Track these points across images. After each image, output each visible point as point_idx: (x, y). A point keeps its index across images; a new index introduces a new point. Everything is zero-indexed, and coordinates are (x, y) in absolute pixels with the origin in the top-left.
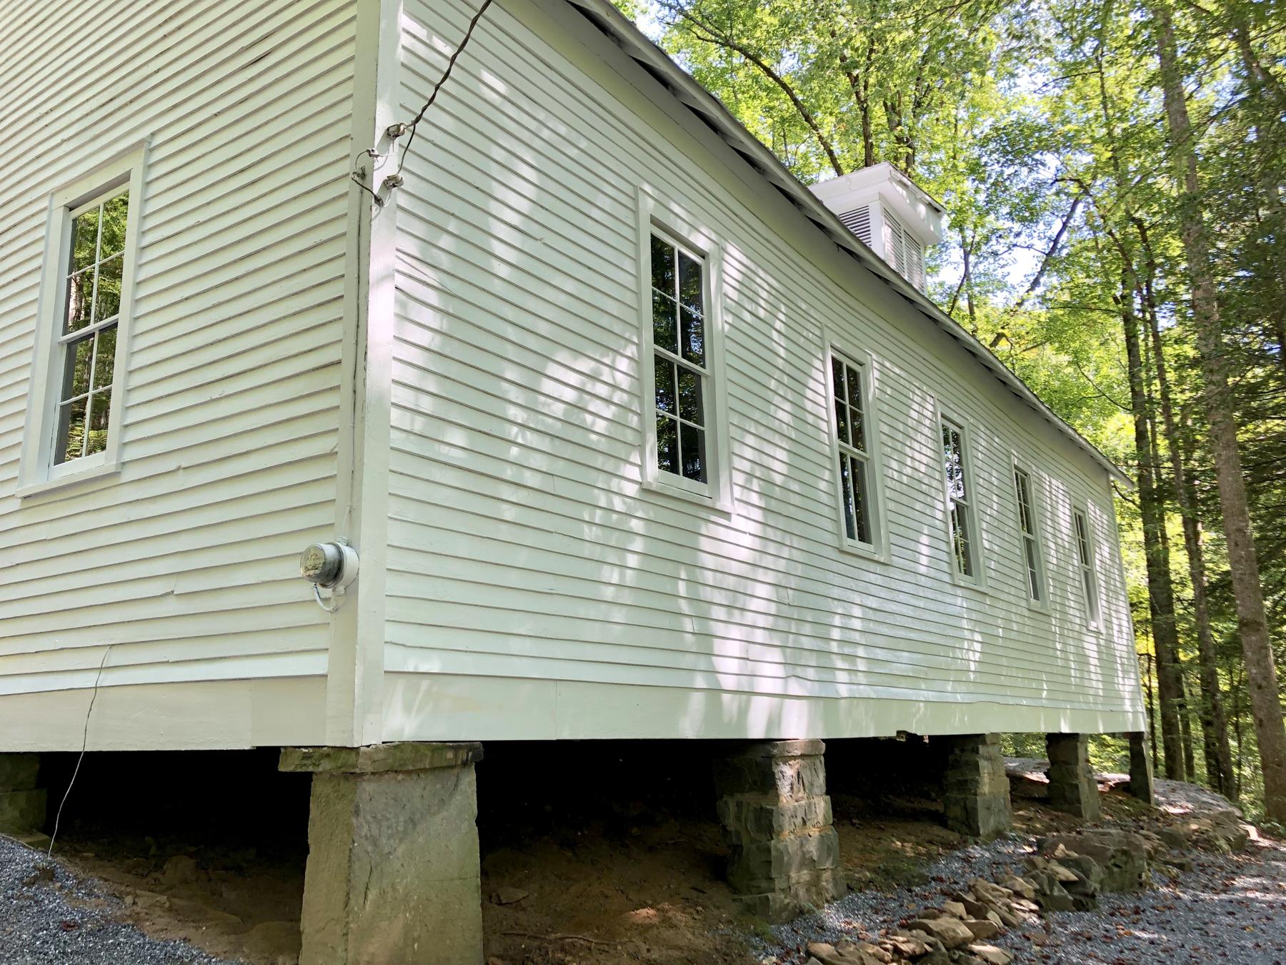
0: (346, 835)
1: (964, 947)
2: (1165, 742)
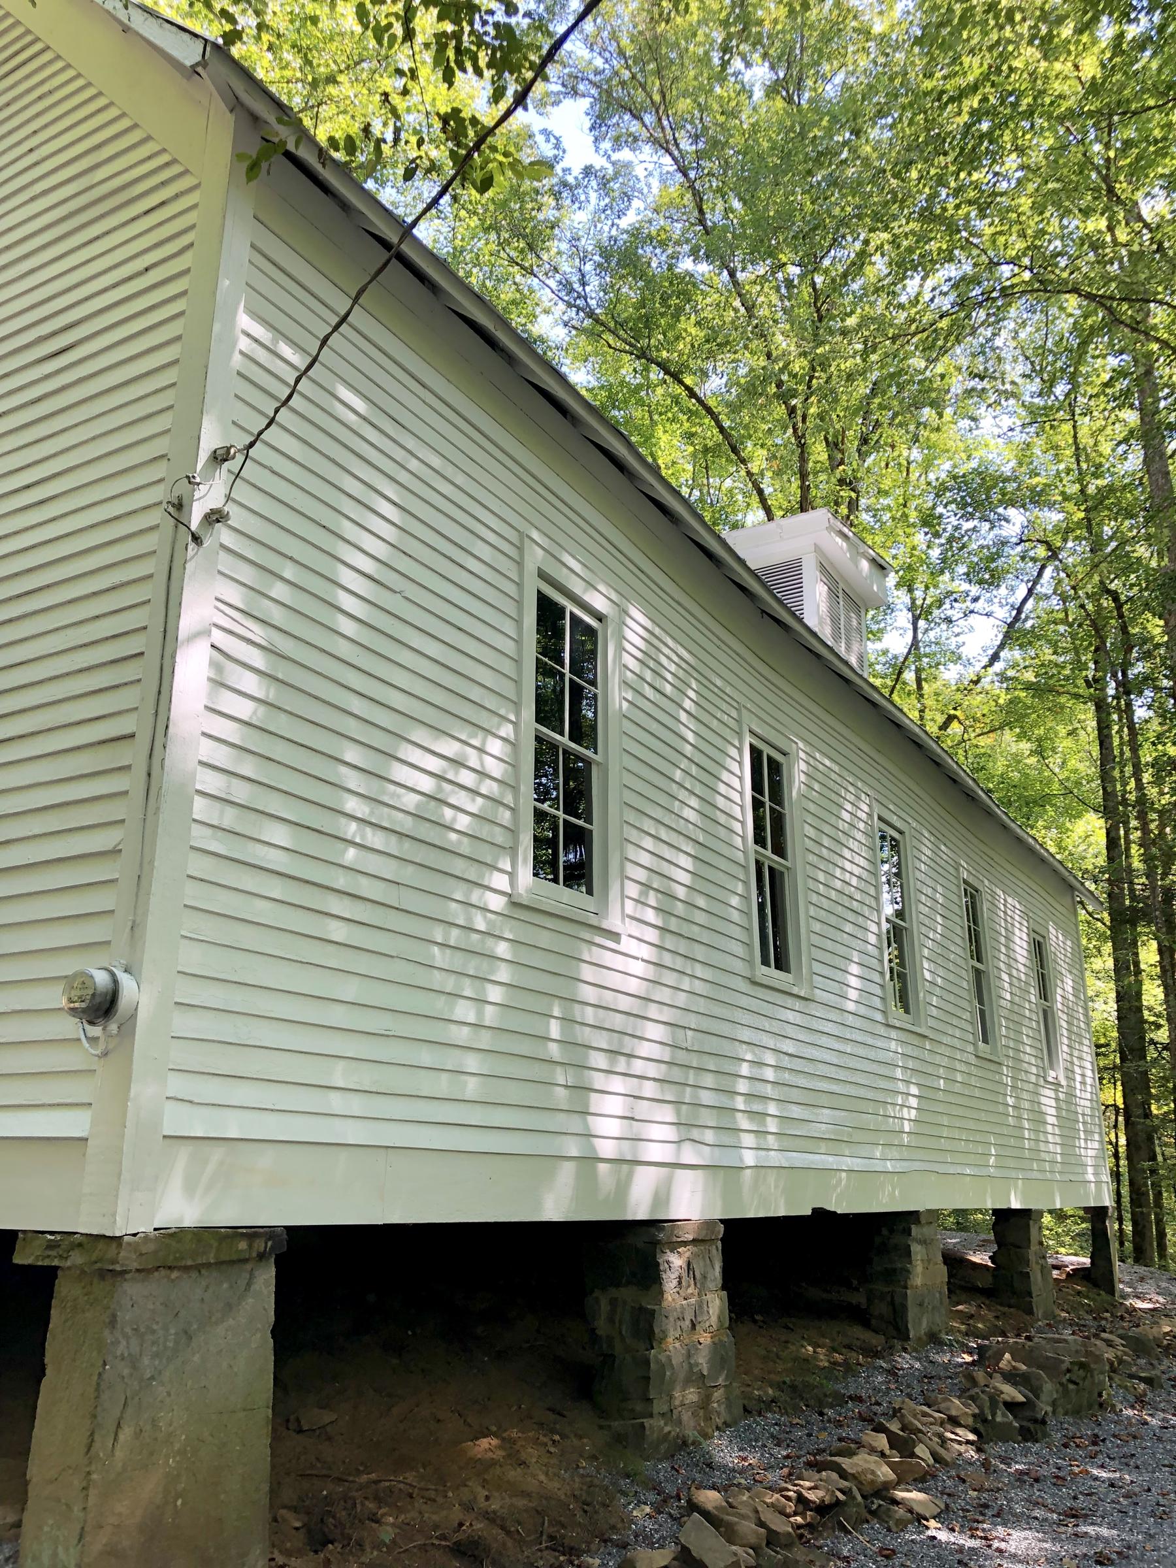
0: (95, 1354)
1: (884, 1493)
2: (1133, 1214)
